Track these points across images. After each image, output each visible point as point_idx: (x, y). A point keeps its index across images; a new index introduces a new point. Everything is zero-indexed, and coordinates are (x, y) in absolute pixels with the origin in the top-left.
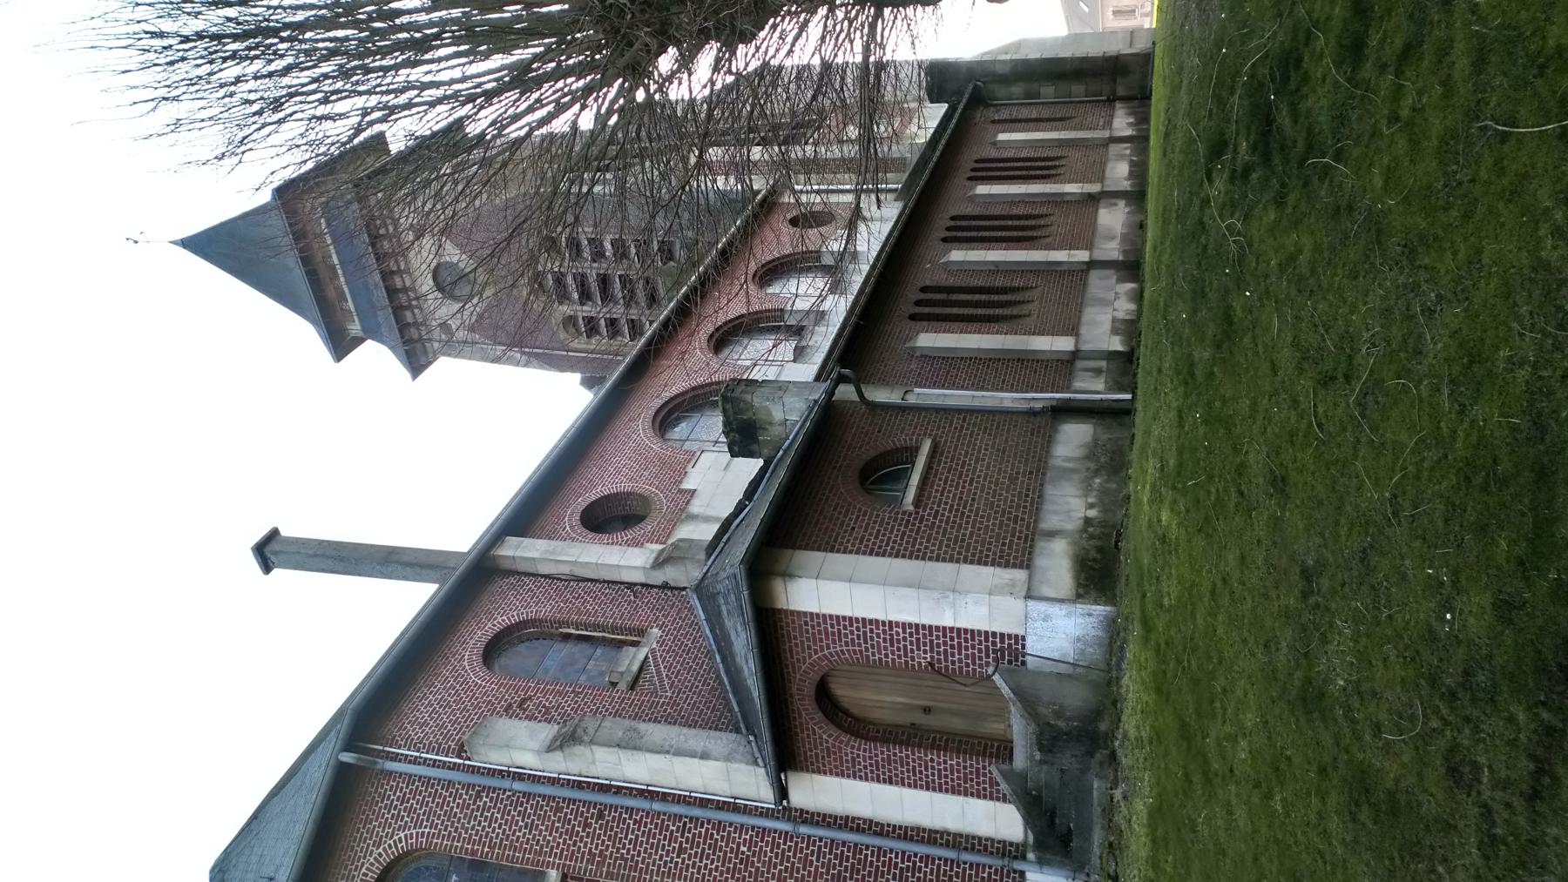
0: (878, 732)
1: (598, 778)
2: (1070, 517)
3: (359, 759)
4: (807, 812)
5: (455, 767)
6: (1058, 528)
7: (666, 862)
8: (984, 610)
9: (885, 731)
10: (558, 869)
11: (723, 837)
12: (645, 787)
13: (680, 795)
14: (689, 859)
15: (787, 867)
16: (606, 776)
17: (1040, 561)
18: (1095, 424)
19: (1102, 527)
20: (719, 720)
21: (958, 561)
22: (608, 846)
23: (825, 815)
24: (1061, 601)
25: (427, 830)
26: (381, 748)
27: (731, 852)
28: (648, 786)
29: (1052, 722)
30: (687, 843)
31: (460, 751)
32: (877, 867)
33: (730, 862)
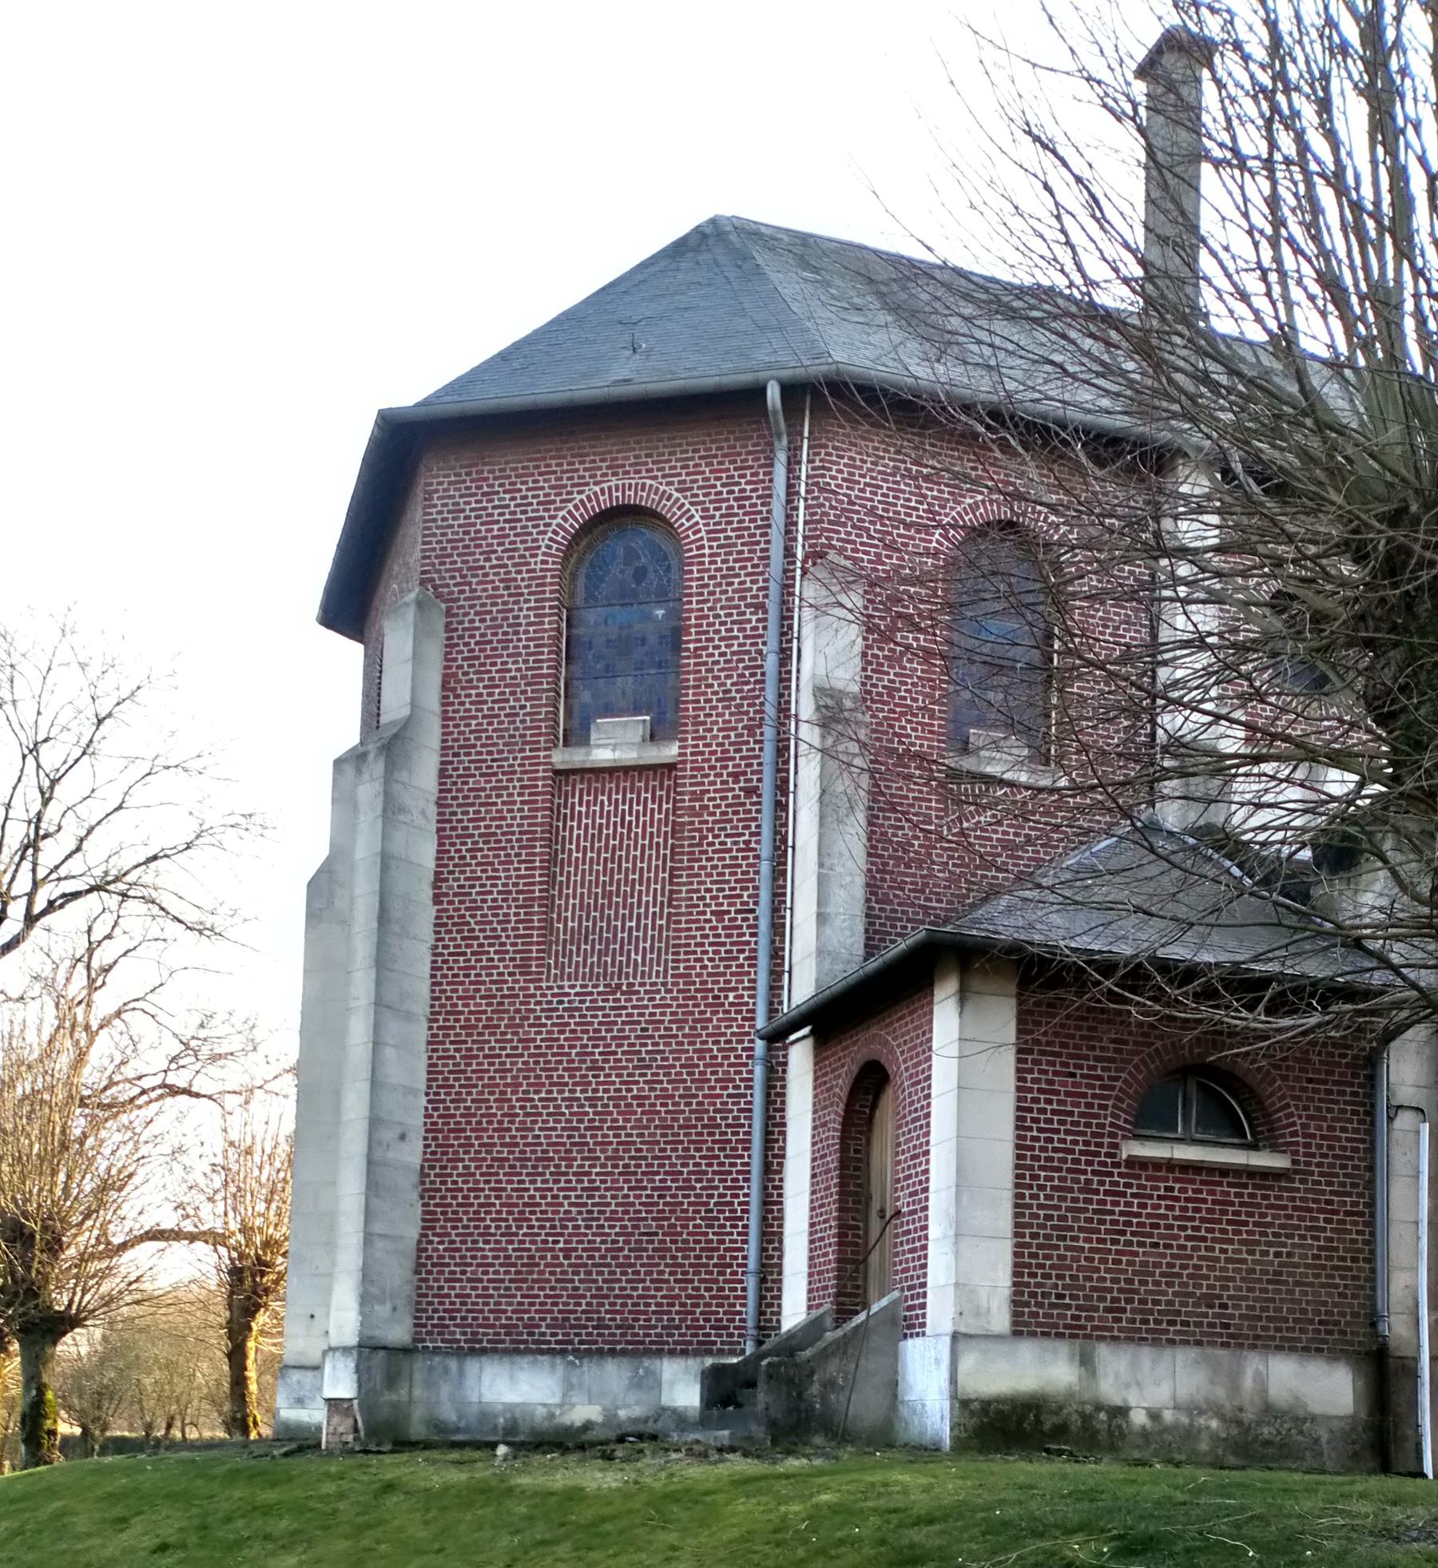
0: (856, 1151)
1: (796, 773)
2: (1127, 1386)
3: (775, 412)
4: (784, 1071)
5: (789, 552)
6: (1100, 1371)
7: (703, 898)
8: (942, 1281)
9: (859, 1160)
10: (680, 755)
11: (742, 966)
12: (790, 843)
13: (785, 895)
14: (711, 929)
15: (716, 1057)
16: (800, 784)
17: (1027, 1350)
18: (1353, 1417)
19: (1110, 1433)
20: (909, 920)
21: (1016, 1235)
22: (714, 814)
23: (784, 1095)
24: (953, 1380)
25: (707, 551)
26: (806, 434)
27: (725, 982)
28: (793, 847)
29: (816, 1377)
30: (730, 920)
31: (816, 555)
32: (730, 1173)
33: (713, 983)
